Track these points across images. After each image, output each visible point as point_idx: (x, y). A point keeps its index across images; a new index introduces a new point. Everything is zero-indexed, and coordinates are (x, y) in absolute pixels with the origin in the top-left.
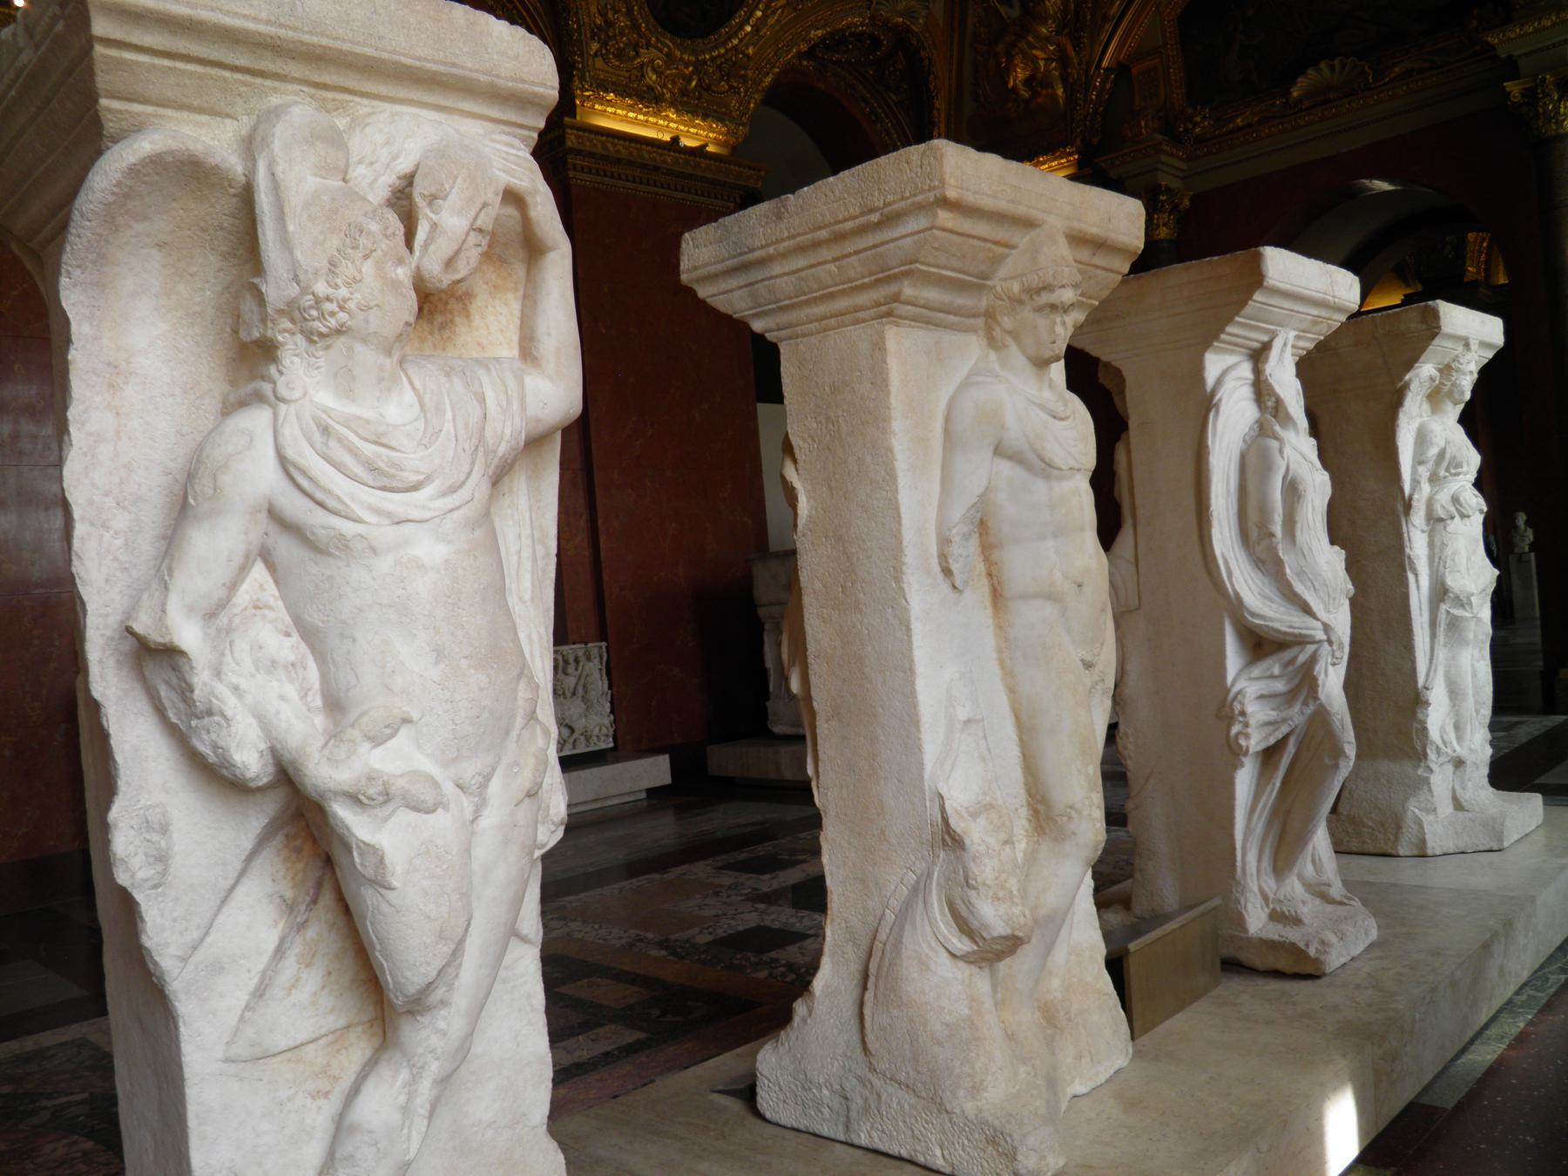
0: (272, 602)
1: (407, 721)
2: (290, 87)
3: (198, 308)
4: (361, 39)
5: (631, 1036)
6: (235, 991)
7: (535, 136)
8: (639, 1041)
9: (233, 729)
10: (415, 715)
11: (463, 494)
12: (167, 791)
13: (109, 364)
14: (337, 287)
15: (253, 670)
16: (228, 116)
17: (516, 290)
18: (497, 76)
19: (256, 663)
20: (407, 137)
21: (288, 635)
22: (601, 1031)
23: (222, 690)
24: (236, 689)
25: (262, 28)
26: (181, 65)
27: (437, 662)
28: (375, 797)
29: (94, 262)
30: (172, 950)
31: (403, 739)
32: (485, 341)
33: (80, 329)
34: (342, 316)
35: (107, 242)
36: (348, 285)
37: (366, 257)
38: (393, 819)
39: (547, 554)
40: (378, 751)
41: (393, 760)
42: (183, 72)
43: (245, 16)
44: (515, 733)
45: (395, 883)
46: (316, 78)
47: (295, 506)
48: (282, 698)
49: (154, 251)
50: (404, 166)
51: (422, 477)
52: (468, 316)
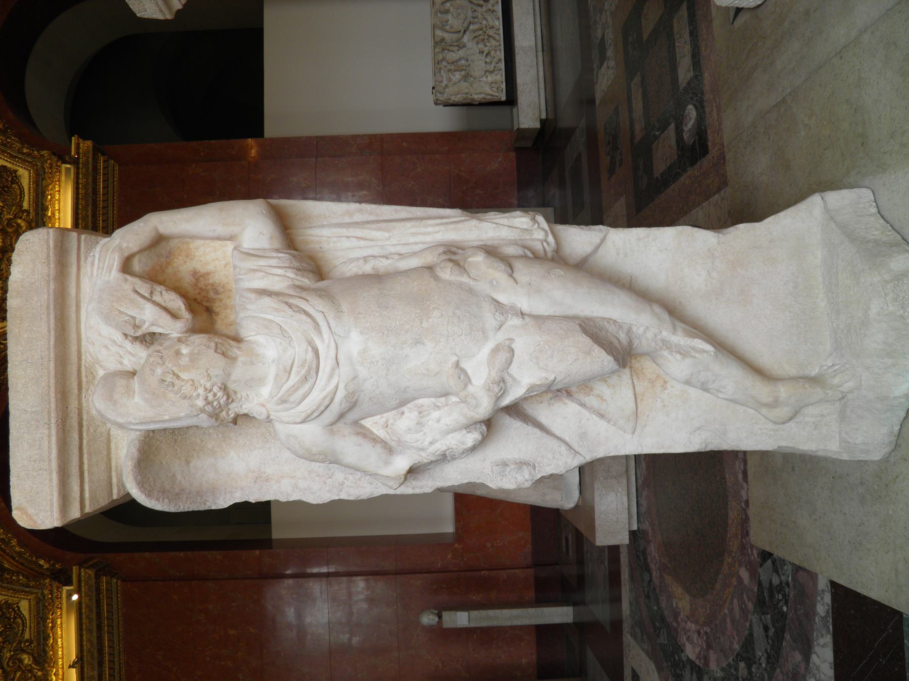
0: (384, 420)
1: (457, 365)
2: (84, 405)
3: (220, 436)
4: (46, 371)
5: (684, 12)
6: (598, 427)
7: (83, 237)
8: (689, 9)
9: (454, 446)
10: (455, 359)
11: (320, 318)
12: (485, 460)
13: (255, 482)
14: (198, 395)
15: (421, 433)
16: (109, 434)
17: (187, 243)
18: (49, 276)
19: (417, 432)
20: (101, 335)
21: (403, 413)
22: (676, 29)
23: (432, 449)
24: (431, 443)
25: (54, 432)
26: (86, 467)
27: (423, 344)
28: (502, 383)
29: (201, 497)
30: (569, 461)
31: (467, 365)
32: (224, 262)
33: (238, 498)
34: (215, 389)
35: (190, 493)
36: (196, 389)
37: (178, 377)
38: (515, 375)
39: (360, 211)
40: (474, 381)
41: (480, 371)
42: (89, 465)
43: (49, 442)
44: (472, 283)
45: (552, 378)
46: (76, 391)
47: (329, 416)
48: (438, 421)
49: (191, 465)
50: (118, 337)
51: (310, 348)
52: (208, 274)
